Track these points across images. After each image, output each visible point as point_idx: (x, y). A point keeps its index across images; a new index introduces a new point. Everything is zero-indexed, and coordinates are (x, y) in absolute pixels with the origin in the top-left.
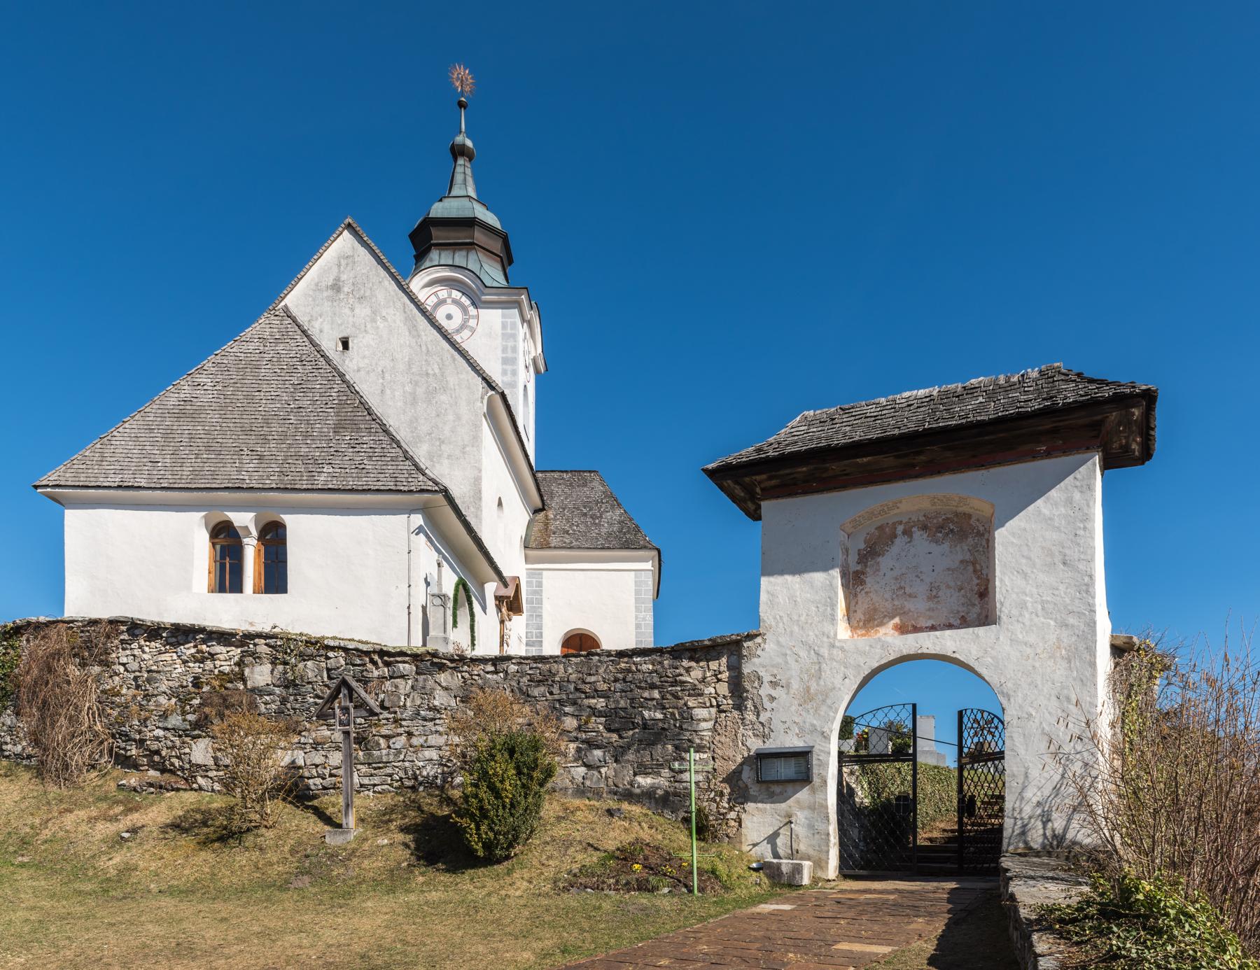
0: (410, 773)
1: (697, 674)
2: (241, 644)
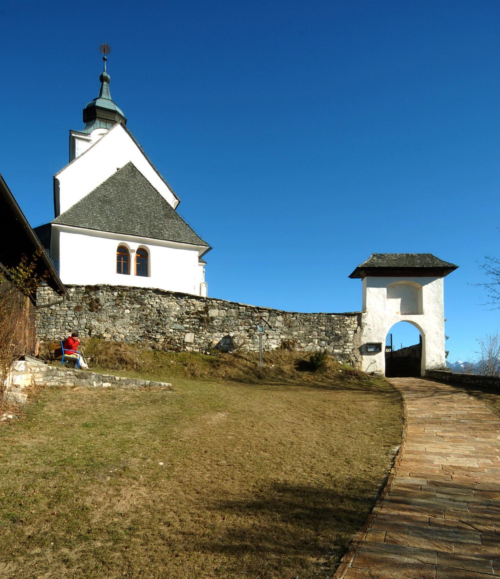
1: (349, 321)
2: (205, 301)
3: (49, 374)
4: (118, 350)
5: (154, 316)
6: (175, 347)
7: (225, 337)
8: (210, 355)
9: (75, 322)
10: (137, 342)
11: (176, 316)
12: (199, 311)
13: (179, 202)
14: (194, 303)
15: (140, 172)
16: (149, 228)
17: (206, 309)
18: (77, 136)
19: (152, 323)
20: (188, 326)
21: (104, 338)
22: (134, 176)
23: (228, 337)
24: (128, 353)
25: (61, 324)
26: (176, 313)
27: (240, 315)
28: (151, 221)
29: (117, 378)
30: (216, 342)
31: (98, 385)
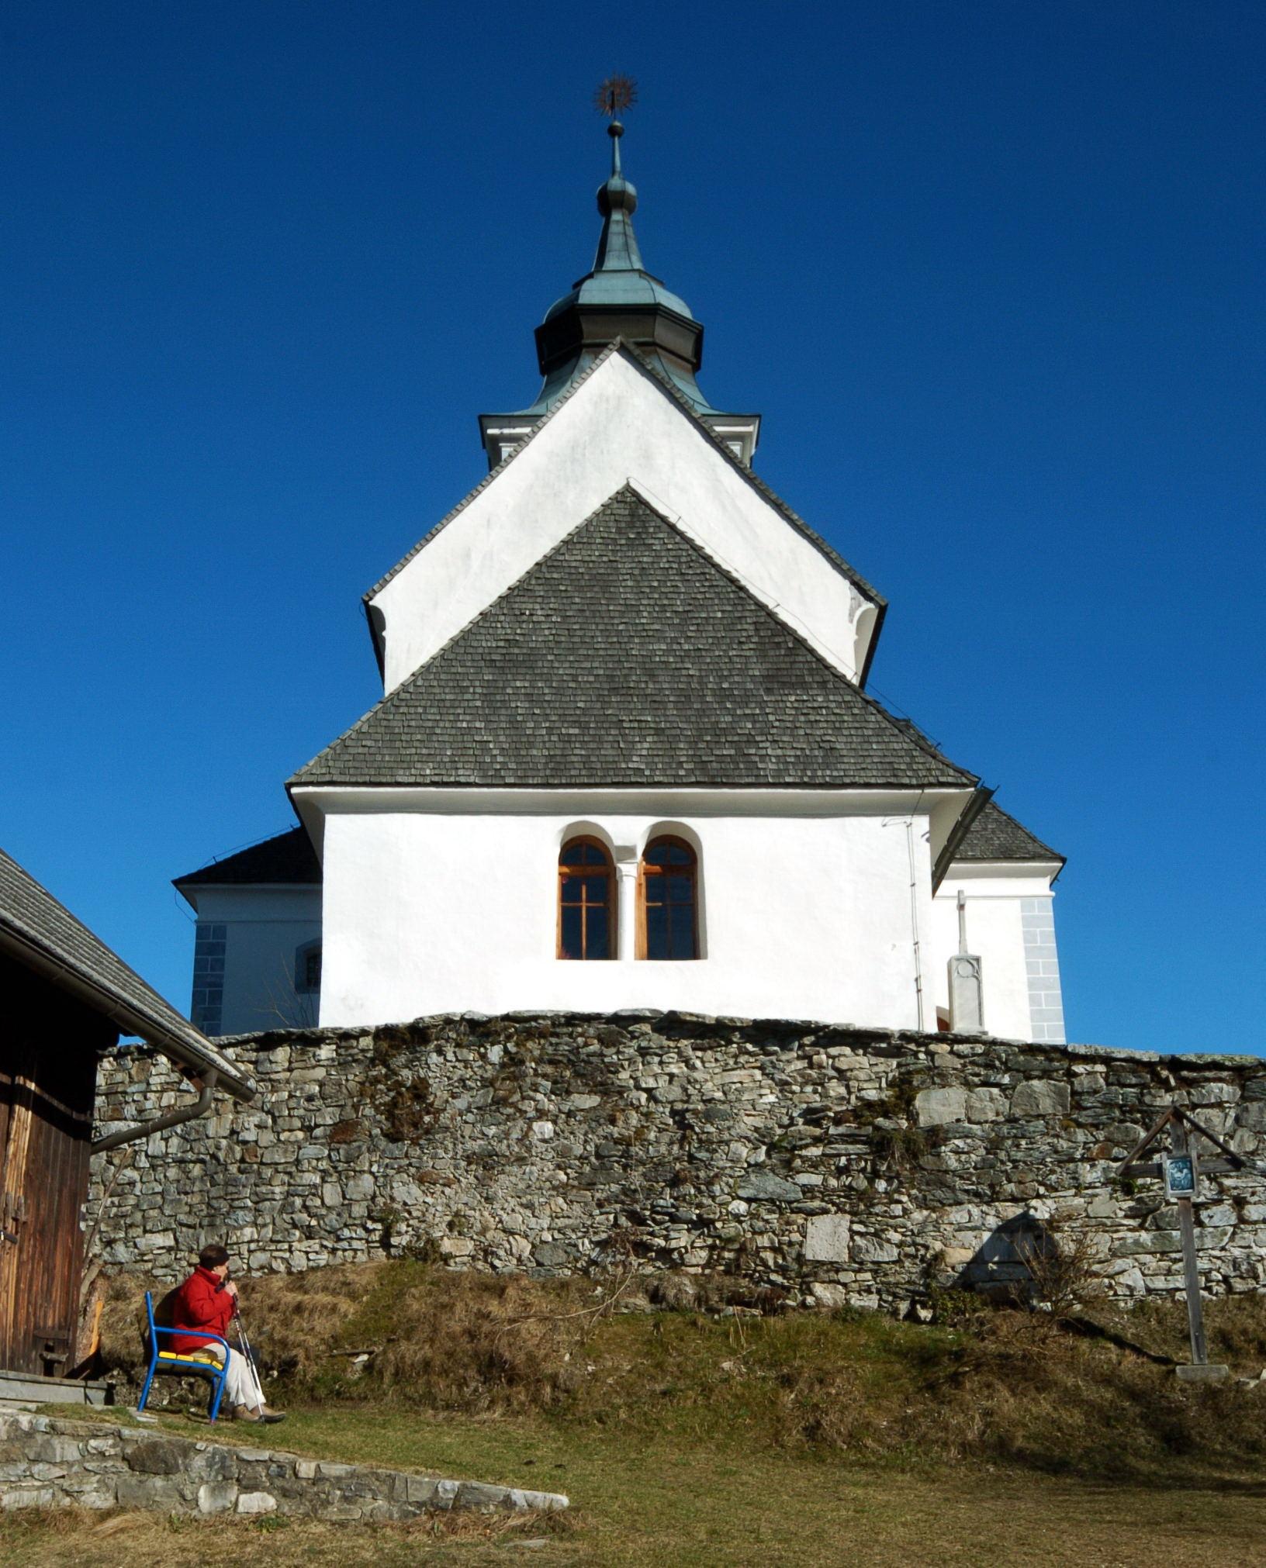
0: (1244, 1267)
2: (895, 1052)
3: (16, 1449)
4: (487, 1316)
5: (661, 1144)
6: (759, 1288)
7: (1008, 1228)
8: (933, 1321)
9: (331, 1194)
10: (586, 1271)
11: (761, 1137)
12: (869, 1105)
13: (882, 611)
14: (843, 1064)
15: (663, 519)
16: (693, 744)
17: (904, 1091)
18: (506, 431)
19: (649, 1179)
20: (815, 1179)
21: (446, 1258)
22: (640, 542)
23: (1026, 1223)
24: (531, 1328)
25: (278, 1205)
26: (759, 1122)
27: (1078, 1107)
28: (702, 713)
29: (307, 1469)
30: (960, 1255)
31: (220, 1503)
